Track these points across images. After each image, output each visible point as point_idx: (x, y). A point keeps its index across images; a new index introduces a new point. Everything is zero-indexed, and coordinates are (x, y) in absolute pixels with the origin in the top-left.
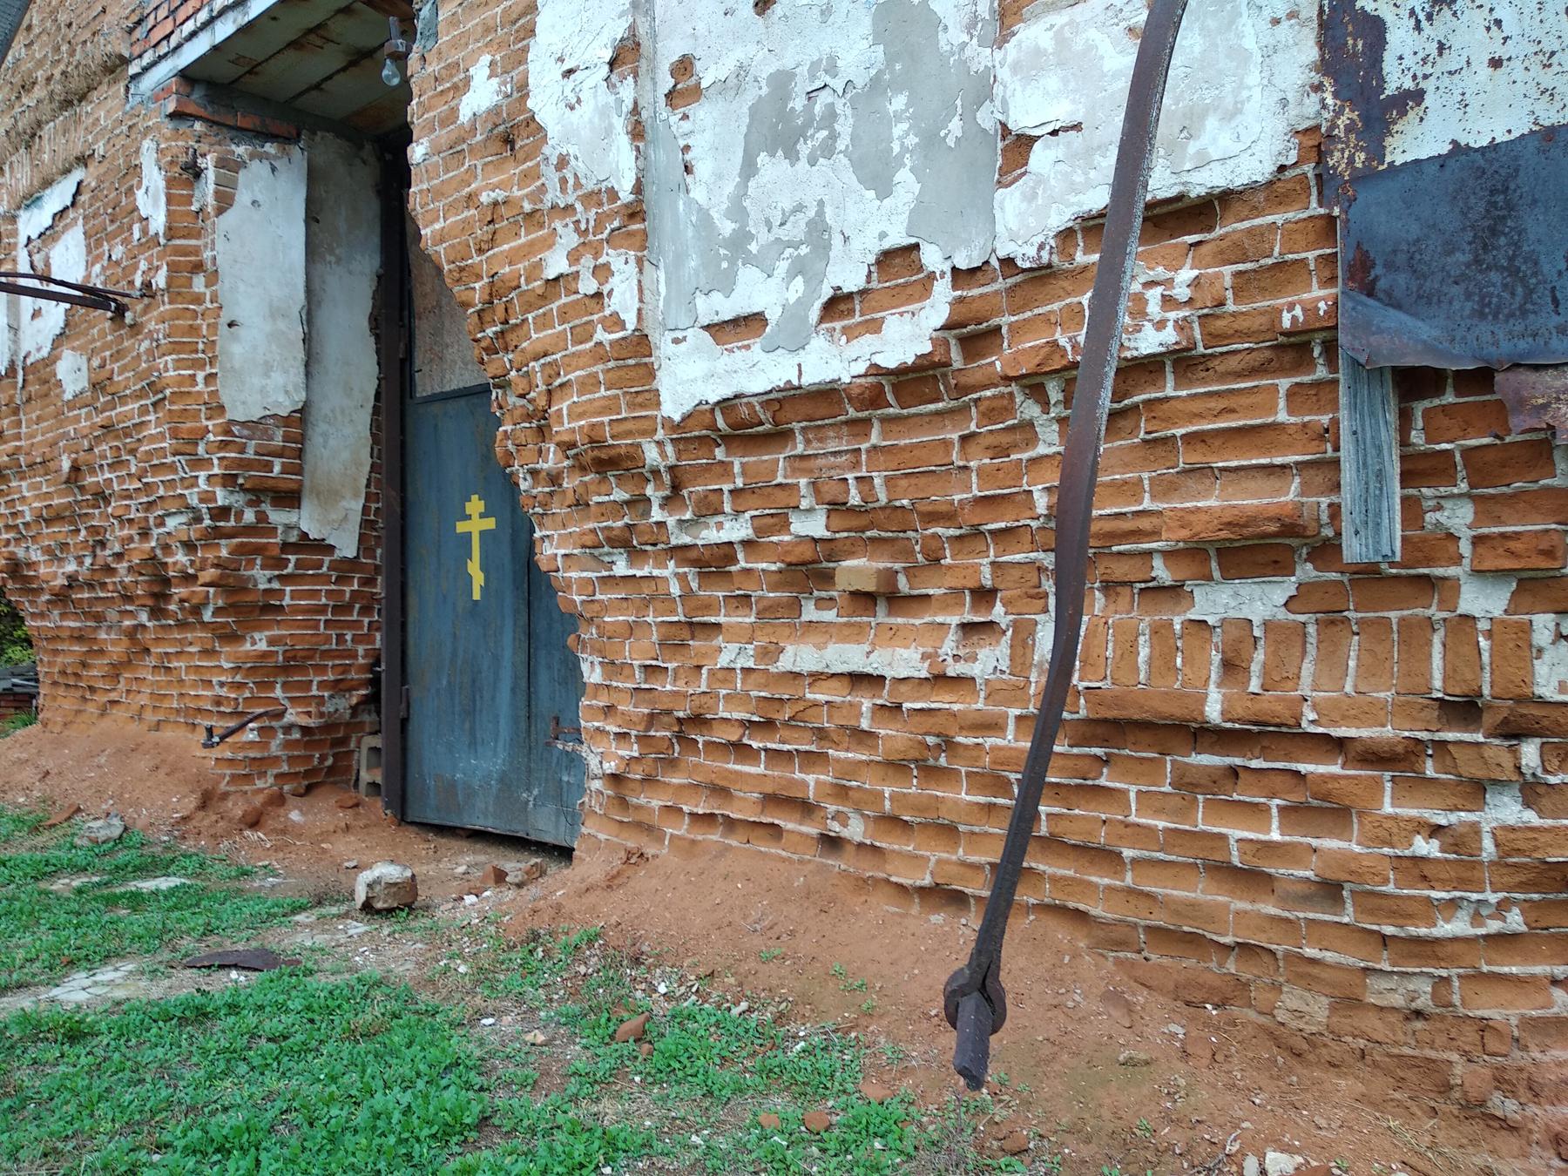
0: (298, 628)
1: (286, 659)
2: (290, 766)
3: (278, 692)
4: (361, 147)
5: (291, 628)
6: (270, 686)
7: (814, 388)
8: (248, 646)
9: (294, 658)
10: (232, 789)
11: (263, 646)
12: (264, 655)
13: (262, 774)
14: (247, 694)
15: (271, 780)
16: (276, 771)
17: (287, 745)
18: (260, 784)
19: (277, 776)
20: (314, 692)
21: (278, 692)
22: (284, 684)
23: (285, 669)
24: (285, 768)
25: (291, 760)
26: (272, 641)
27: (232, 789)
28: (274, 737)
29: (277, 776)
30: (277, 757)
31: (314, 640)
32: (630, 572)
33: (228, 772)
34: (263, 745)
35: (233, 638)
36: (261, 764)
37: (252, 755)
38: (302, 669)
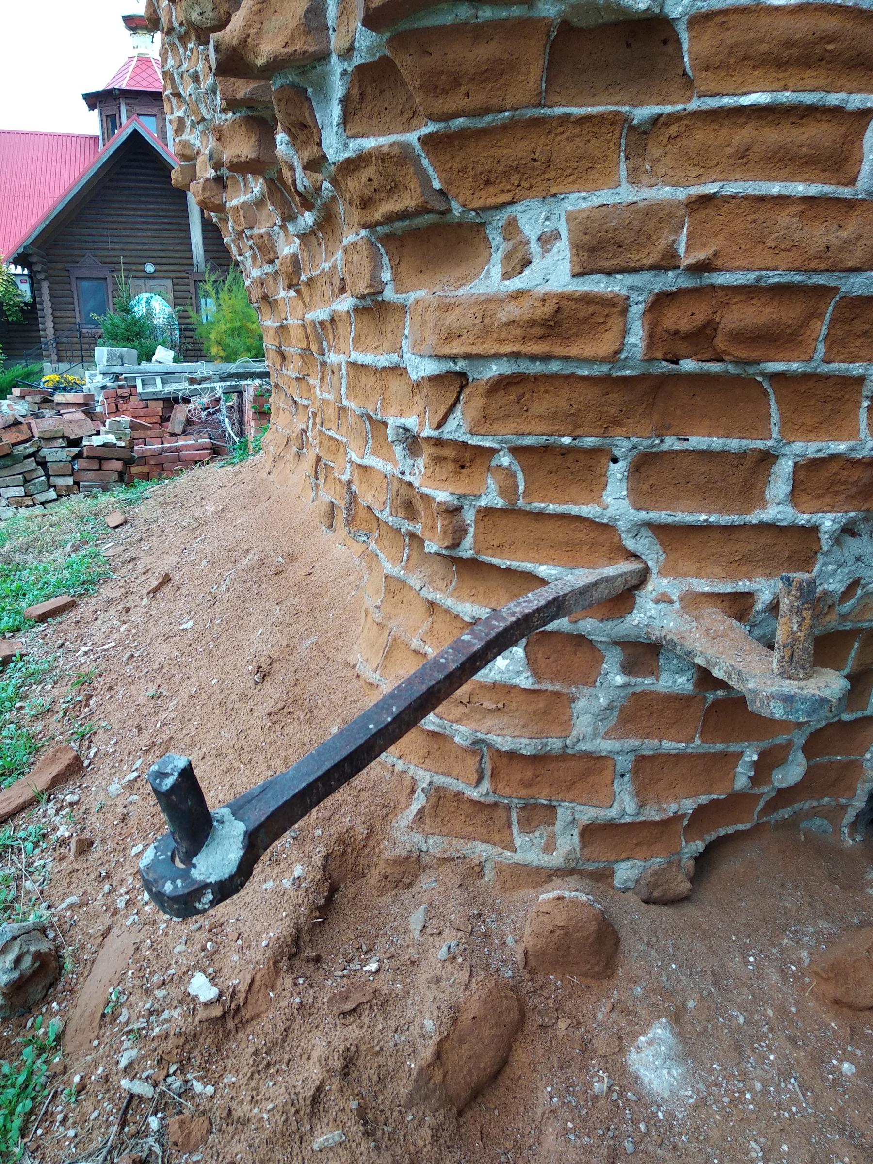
0: (743, 160)
1: (665, 343)
2: (641, 797)
3: (614, 500)
4: (640, 182)
5: (702, 163)
6: (580, 467)
7: (246, 841)
8: (491, 279)
9: (701, 339)
10: (435, 845)
11: (554, 273)
12: (561, 320)
13: (538, 815)
14: (492, 498)
15: (568, 843)
16: (588, 814)
17: (636, 712)
18: (528, 849)
19: (591, 833)
20: (776, 507)
21: (614, 500)
22: (644, 464)
23: (650, 393)
24: (624, 805)
25: (645, 767)
26: (599, 248)
27: (435, 845)
28: (589, 676)
29: (591, 833)
30: (595, 762)
31: (820, 234)
32: (536, 687)
33: (424, 777)
34: (550, 707)
35: (433, 237)
36: (539, 777)
37: (504, 743)
38: (733, 395)
